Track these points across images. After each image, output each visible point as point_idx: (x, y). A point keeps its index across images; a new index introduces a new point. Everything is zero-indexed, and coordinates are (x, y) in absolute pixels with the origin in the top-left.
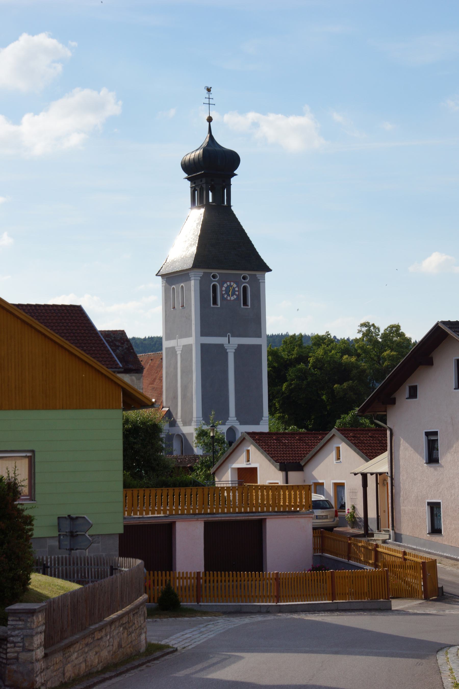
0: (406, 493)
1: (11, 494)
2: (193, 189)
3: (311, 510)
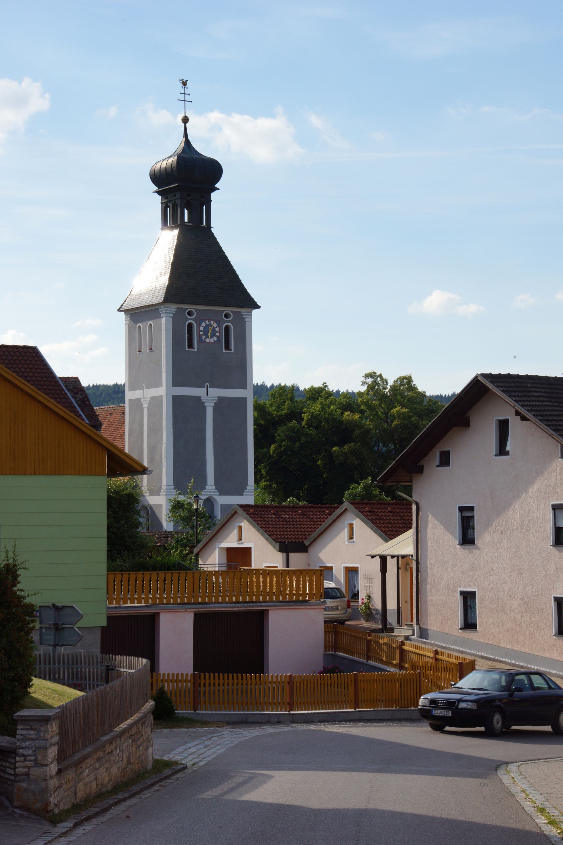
0: (434, 580)
1: (10, 577)
2: (164, 205)
3: (322, 600)
